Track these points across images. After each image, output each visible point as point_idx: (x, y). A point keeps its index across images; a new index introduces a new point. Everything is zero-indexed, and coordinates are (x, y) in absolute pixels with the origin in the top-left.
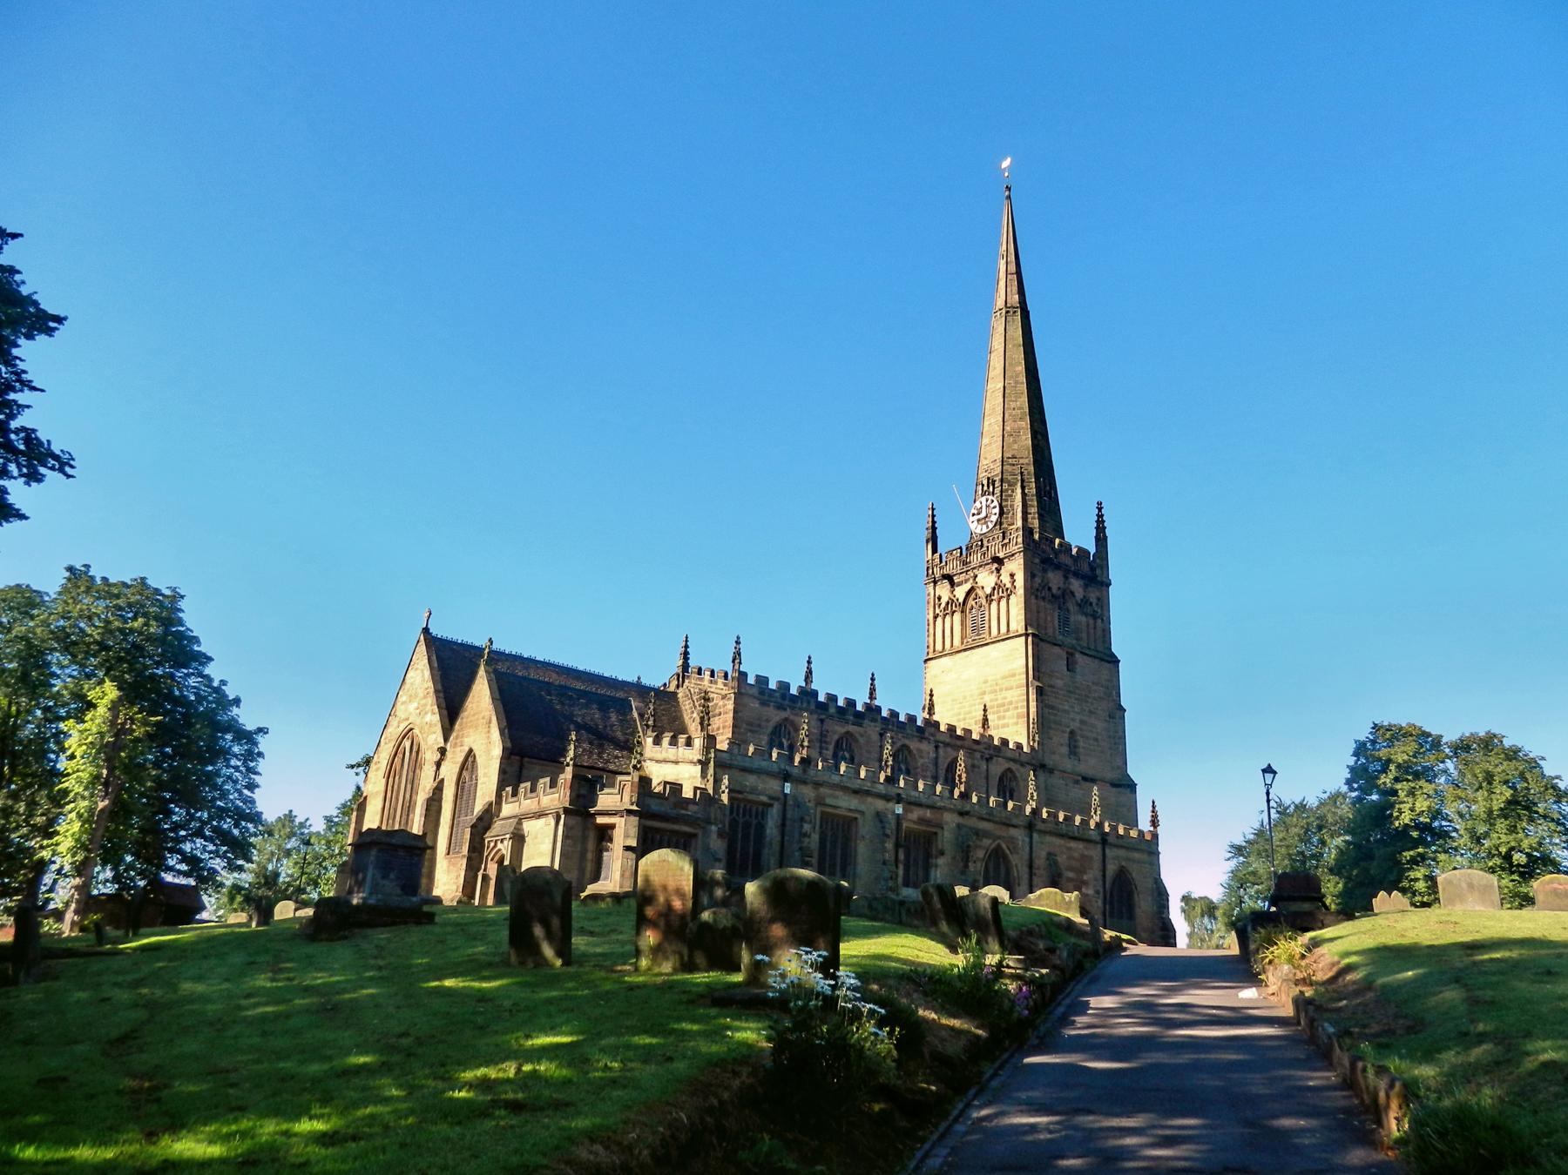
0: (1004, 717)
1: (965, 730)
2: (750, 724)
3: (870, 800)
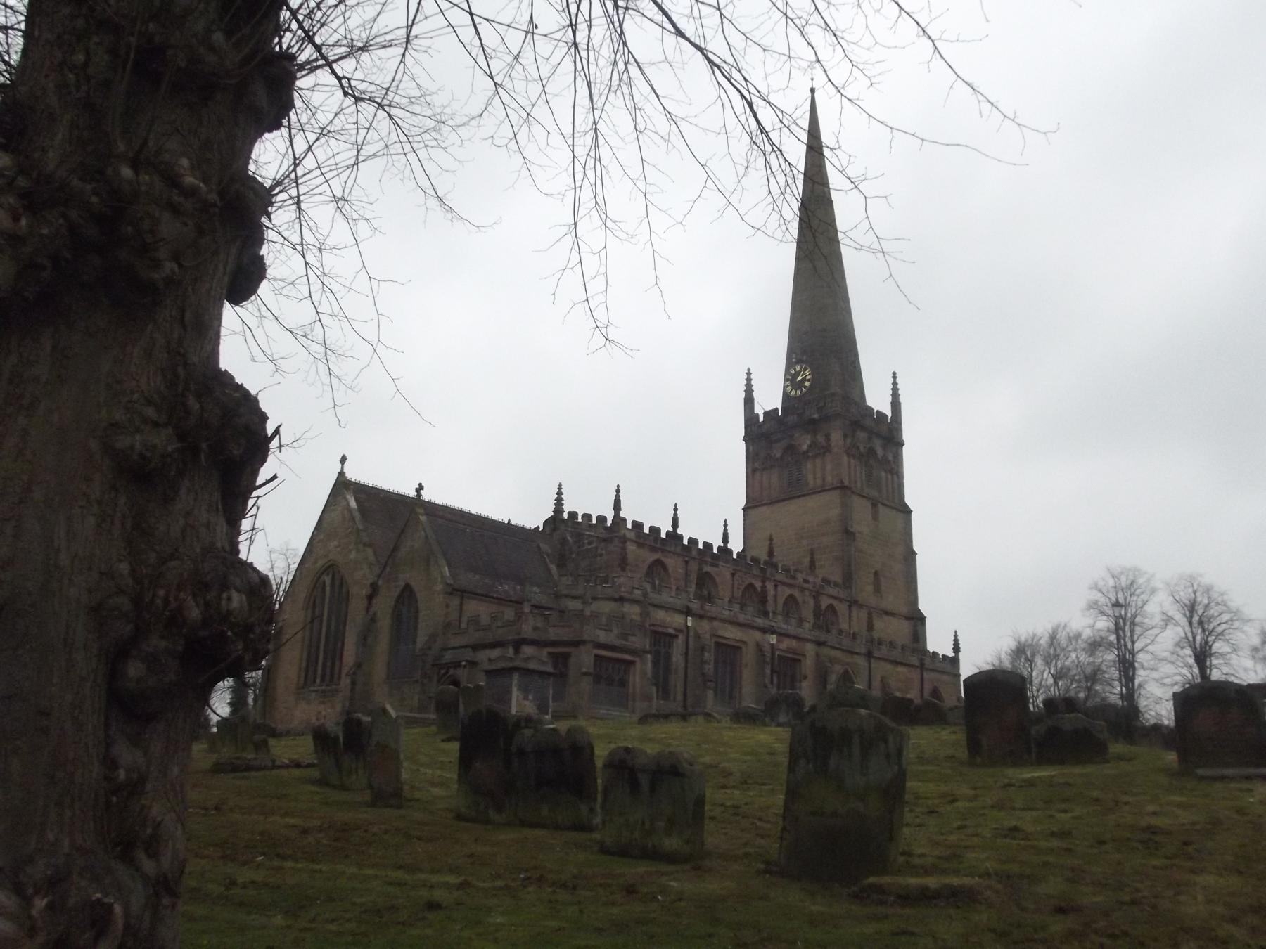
1: (652, 529)
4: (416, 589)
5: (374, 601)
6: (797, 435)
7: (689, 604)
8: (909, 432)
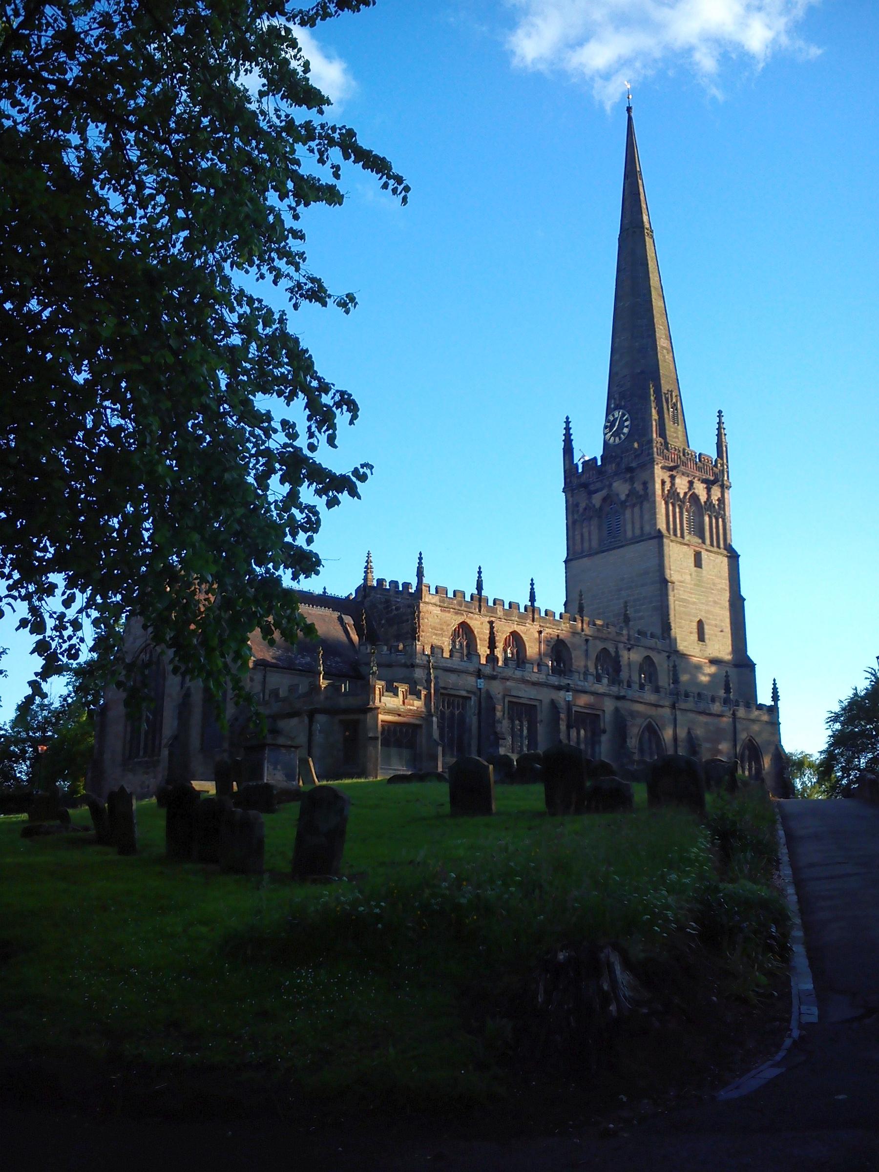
2: (434, 628)
6: (615, 485)
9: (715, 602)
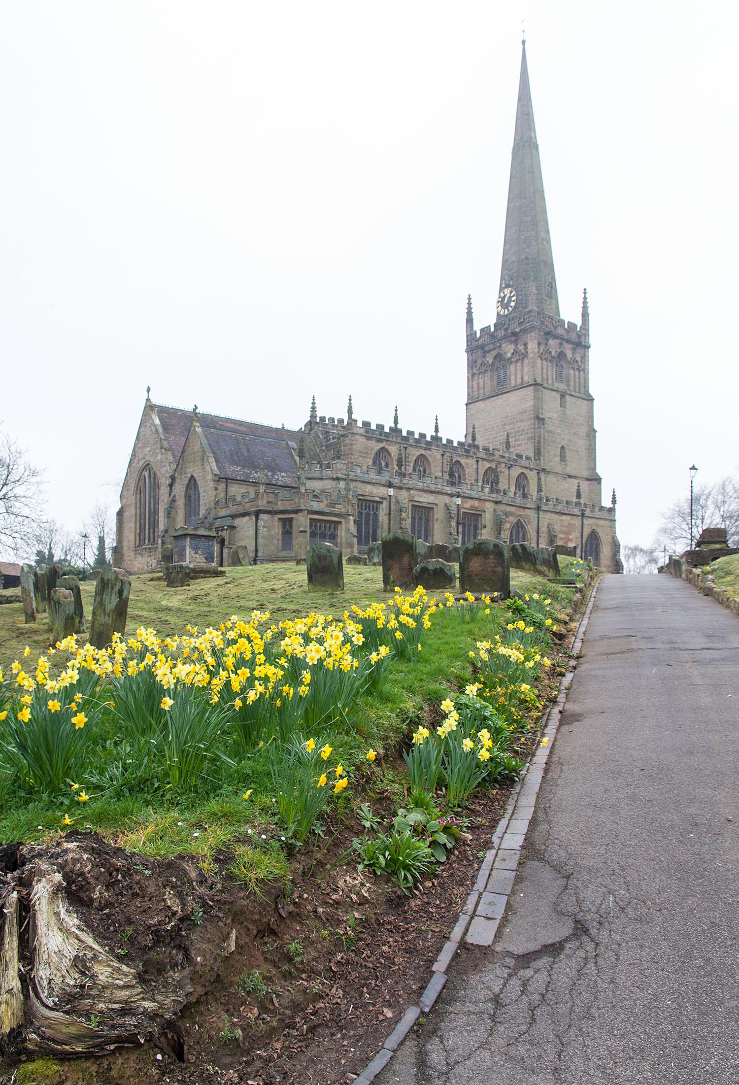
0: (519, 440)
1: (378, 426)
2: (360, 452)
3: (441, 496)
4: (197, 479)
5: (173, 488)
6: (503, 346)
7: (391, 480)
8: (594, 339)
9: (575, 434)
